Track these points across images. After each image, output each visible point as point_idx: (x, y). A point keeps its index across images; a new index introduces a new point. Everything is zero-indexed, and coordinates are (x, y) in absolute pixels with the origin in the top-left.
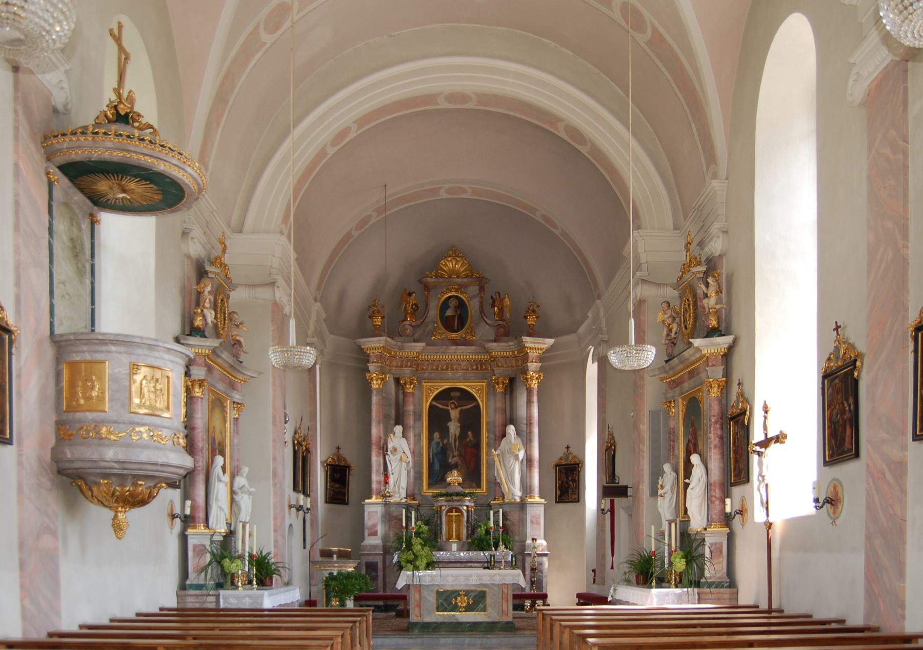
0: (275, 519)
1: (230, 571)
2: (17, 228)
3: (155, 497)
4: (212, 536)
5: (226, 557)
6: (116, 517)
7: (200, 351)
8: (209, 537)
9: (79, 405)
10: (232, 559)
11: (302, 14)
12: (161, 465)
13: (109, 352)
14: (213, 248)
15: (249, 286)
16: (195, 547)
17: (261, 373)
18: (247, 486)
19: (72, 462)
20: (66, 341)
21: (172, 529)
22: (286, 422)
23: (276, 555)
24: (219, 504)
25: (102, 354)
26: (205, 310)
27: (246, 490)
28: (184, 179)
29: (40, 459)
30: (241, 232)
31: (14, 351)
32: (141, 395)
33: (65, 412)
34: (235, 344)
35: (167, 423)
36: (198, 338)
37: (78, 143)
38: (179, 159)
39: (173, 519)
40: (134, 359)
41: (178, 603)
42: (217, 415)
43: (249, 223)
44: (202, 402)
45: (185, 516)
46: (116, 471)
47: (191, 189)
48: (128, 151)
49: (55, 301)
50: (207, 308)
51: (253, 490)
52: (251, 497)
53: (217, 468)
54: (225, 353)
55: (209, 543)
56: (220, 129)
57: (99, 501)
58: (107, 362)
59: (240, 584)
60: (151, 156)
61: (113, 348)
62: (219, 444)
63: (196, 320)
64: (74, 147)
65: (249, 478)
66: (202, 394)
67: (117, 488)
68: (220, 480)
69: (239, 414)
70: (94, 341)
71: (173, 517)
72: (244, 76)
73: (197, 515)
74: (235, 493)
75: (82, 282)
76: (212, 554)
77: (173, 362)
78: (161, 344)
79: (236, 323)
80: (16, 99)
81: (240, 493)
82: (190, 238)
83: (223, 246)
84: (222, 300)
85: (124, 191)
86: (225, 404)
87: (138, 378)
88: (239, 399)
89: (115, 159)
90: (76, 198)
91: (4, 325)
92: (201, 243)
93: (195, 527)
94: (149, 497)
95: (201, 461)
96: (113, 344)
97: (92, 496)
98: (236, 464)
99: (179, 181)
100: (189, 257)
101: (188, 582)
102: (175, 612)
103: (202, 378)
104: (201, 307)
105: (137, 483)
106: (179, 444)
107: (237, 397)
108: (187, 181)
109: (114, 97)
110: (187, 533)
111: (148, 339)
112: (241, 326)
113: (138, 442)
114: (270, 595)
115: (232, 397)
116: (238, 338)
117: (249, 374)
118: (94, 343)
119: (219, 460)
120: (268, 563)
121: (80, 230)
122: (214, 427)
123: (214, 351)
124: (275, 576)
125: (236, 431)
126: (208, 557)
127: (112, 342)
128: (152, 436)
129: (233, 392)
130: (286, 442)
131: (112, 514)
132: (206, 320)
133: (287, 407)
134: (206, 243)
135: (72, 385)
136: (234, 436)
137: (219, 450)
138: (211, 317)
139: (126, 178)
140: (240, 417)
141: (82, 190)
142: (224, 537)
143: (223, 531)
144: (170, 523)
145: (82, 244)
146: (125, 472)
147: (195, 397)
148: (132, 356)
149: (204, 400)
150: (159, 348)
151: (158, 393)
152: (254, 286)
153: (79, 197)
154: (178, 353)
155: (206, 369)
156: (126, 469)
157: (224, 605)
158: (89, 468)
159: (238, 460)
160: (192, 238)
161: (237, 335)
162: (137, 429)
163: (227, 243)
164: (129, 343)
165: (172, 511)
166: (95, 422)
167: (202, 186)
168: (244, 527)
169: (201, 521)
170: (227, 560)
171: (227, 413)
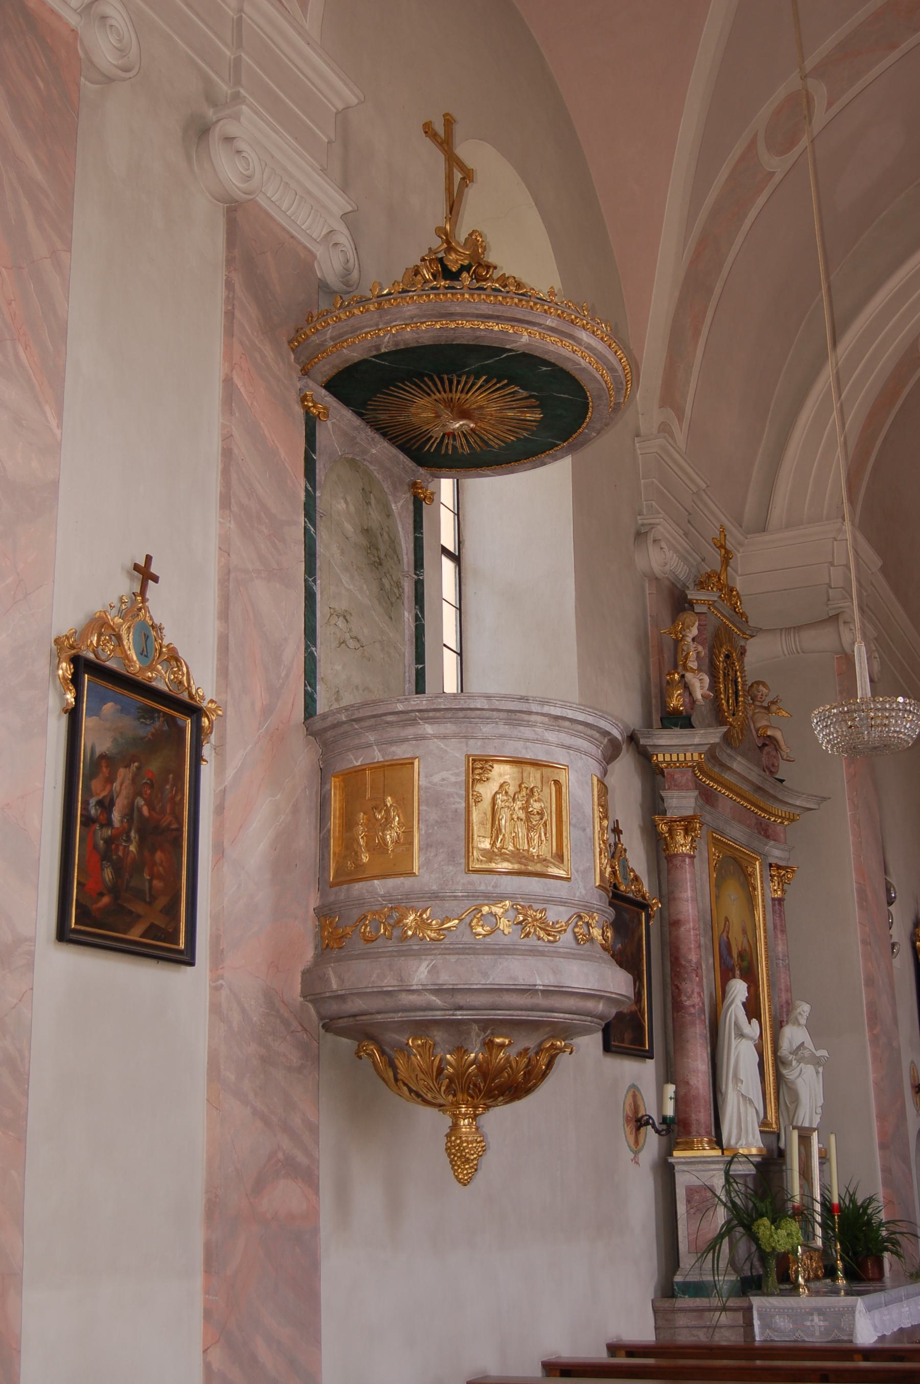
0: (881, 1117)
1: (774, 1249)
2: (225, 502)
3: (544, 1075)
4: (730, 1163)
5: (762, 1216)
6: (455, 1127)
7: (675, 758)
8: (722, 1166)
9: (359, 866)
10: (777, 1217)
11: (835, 109)
12: (543, 991)
13: (423, 738)
14: (703, 560)
15: (788, 629)
16: (691, 1191)
17: (825, 799)
18: (809, 1044)
19: (341, 998)
20: (334, 726)
21: (636, 1153)
22: (890, 903)
23: (889, 1202)
24: (743, 1088)
25: (405, 746)
26: (689, 676)
27: (807, 1053)
28: (577, 358)
29: (271, 999)
30: (764, 530)
31: (207, 751)
32: (496, 830)
33: (332, 886)
34: (764, 745)
35: (560, 890)
36: (677, 731)
37: (352, 321)
38: (559, 315)
39: (638, 1129)
40: (475, 747)
41: (656, 1328)
42: (733, 893)
43: (778, 511)
44: (692, 864)
45: (665, 1120)
46: (438, 1015)
47: (598, 381)
48: (450, 316)
49: (320, 651)
50: (692, 670)
51: (823, 1053)
52: (821, 1070)
53: (733, 1007)
54: (739, 759)
55: (722, 1181)
56: (702, 341)
57: (411, 1090)
58: (416, 762)
59: (801, 1280)
60: (498, 318)
61: (429, 729)
62: (740, 955)
63: (671, 697)
64: (346, 333)
65: (810, 1027)
66: (693, 848)
67: (448, 1056)
68: (741, 1035)
69: (783, 890)
70: (389, 718)
71: (639, 1122)
72: (739, 239)
73: (694, 1117)
74: (783, 1063)
75: (392, 617)
76: (733, 1207)
77: (569, 748)
78: (535, 708)
79: (765, 704)
80: (230, 262)
81: (794, 1063)
82: (650, 541)
83: (723, 551)
84: (727, 657)
85: (464, 414)
86: (750, 869)
87: (486, 791)
88: (780, 859)
89: (427, 340)
90: (374, 451)
91: (185, 696)
92: (676, 551)
93: (689, 1146)
94: (528, 1074)
95: (695, 995)
96: (427, 720)
97: (396, 1080)
98: (784, 996)
99: (568, 367)
100: (655, 579)
101: (678, 1278)
102: (650, 1361)
103: (690, 813)
104: (680, 669)
105: (492, 1041)
106: (592, 940)
107: (776, 854)
108: (584, 363)
109: (437, 243)
110: (671, 1160)
111: (504, 697)
112: (774, 708)
113: (488, 939)
114: (869, 1309)
115: (765, 856)
116: (769, 733)
117: (798, 803)
118: (387, 723)
119: (739, 989)
120: (869, 1223)
121: (389, 515)
122: (727, 919)
123: (712, 754)
124: (886, 1255)
125: (780, 926)
126: (721, 1215)
127: (426, 715)
128: (520, 923)
129: (766, 845)
130: (893, 945)
131: (449, 1122)
132: (690, 694)
133: (891, 869)
134: (687, 552)
135: (348, 823)
136: (776, 937)
137: (741, 970)
138: (702, 687)
139: (459, 382)
140: (786, 897)
141: (384, 431)
142: (757, 1165)
143: (754, 1151)
144: (632, 1139)
145: (393, 543)
146: (459, 1015)
147: (676, 855)
148: (471, 742)
149: (696, 860)
150: (533, 718)
151: (535, 819)
152: (798, 628)
153: (381, 449)
154: (580, 728)
155: (696, 793)
156: (460, 1008)
157: (762, 1333)
158: (378, 1013)
159: (788, 990)
160: (655, 541)
161: (767, 727)
162: (485, 909)
163: (729, 546)
164: (461, 714)
165: (636, 1108)
166: (390, 901)
167: (620, 372)
168: (805, 1140)
169: (703, 1131)
170: (766, 1221)
171: (755, 889)
